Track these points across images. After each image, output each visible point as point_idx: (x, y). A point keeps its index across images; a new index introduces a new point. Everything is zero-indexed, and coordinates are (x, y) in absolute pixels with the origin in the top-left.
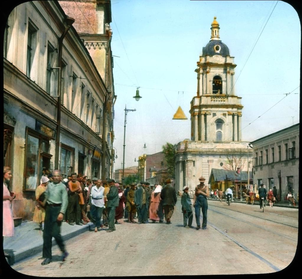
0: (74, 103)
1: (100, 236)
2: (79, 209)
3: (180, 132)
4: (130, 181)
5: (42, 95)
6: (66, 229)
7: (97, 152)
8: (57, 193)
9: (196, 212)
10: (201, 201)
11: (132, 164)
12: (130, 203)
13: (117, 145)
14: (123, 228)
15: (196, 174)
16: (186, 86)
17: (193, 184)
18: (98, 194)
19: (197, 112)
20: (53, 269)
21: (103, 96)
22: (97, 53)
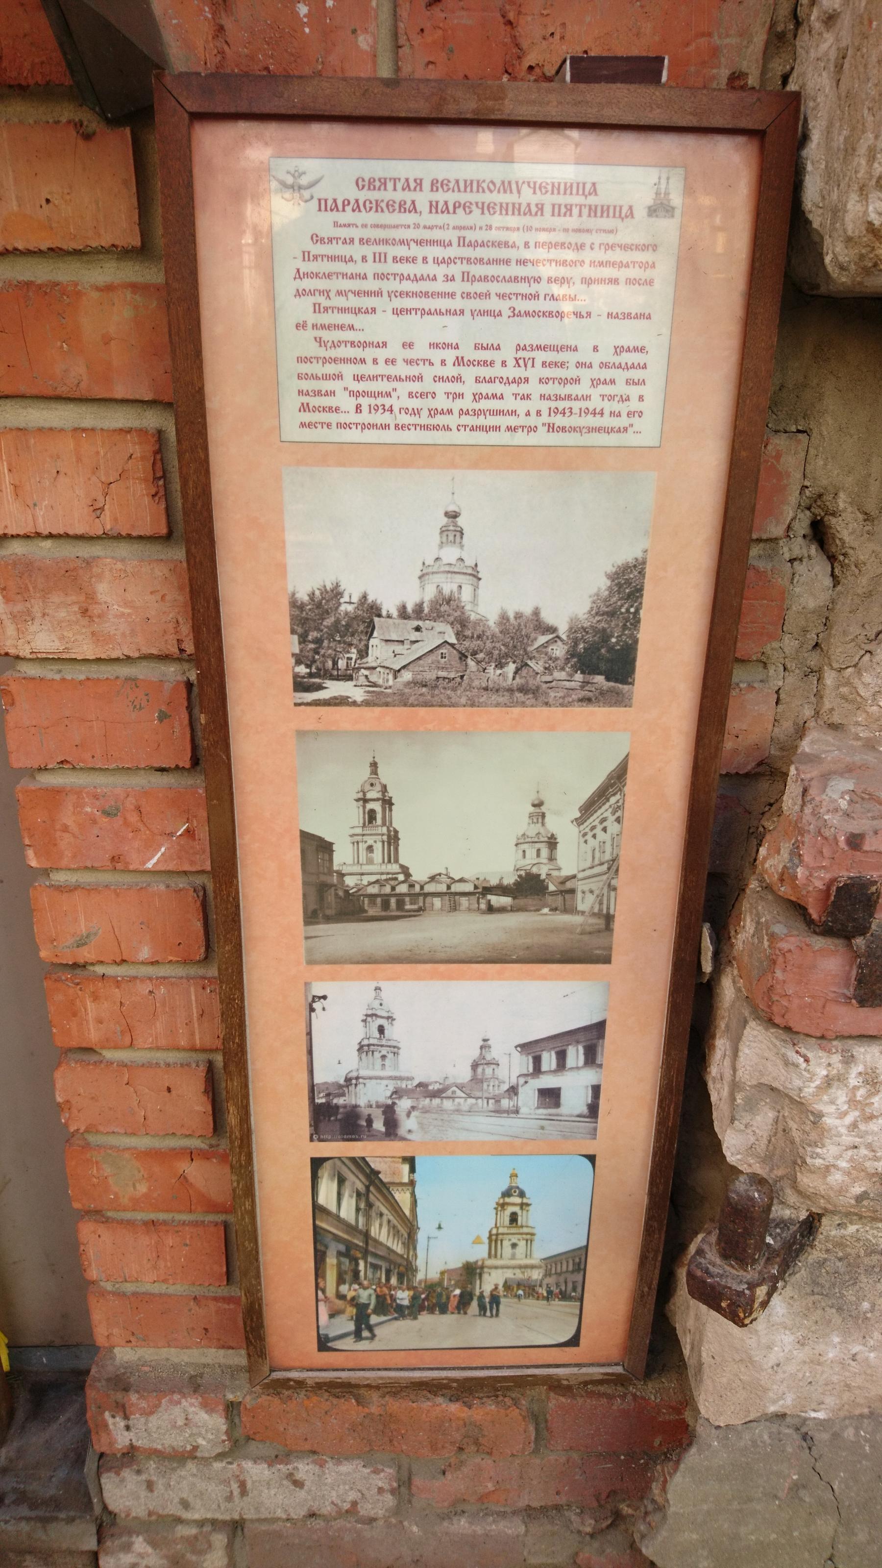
0: (381, 1233)
1: (405, 1324)
2: (385, 1305)
3: (479, 1253)
4: (431, 1287)
5: (351, 1229)
6: (374, 1319)
7: (404, 1269)
8: (366, 1296)
9: (491, 1305)
10: (495, 1299)
11: (433, 1275)
12: (432, 1300)
13: (420, 1263)
14: (425, 1318)
15: (490, 1282)
16: (486, 1220)
17: (487, 1288)
18: (403, 1297)
19: (494, 1239)
20: (363, 1345)
21: (408, 1229)
22: (402, 1198)
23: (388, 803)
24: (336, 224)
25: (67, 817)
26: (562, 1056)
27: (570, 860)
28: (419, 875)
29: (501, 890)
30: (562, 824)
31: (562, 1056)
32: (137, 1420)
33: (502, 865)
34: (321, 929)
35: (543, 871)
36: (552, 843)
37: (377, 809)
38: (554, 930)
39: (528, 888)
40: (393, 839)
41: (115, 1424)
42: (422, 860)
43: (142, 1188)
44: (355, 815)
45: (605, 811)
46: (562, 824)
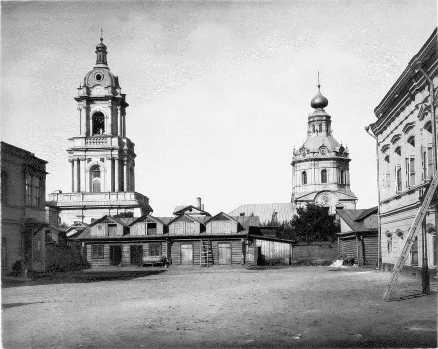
23: (119, 103)
26: (211, 257)
27: (370, 185)
28: (162, 210)
29: (275, 232)
30: (352, 128)
31: (211, 257)
33: (274, 194)
34: (26, 292)
35: (332, 203)
36: (342, 161)
37: (105, 110)
38: (352, 294)
39: (313, 228)
40: (126, 156)
42: (168, 185)
44: (75, 121)
45: (410, 113)
46: (352, 128)
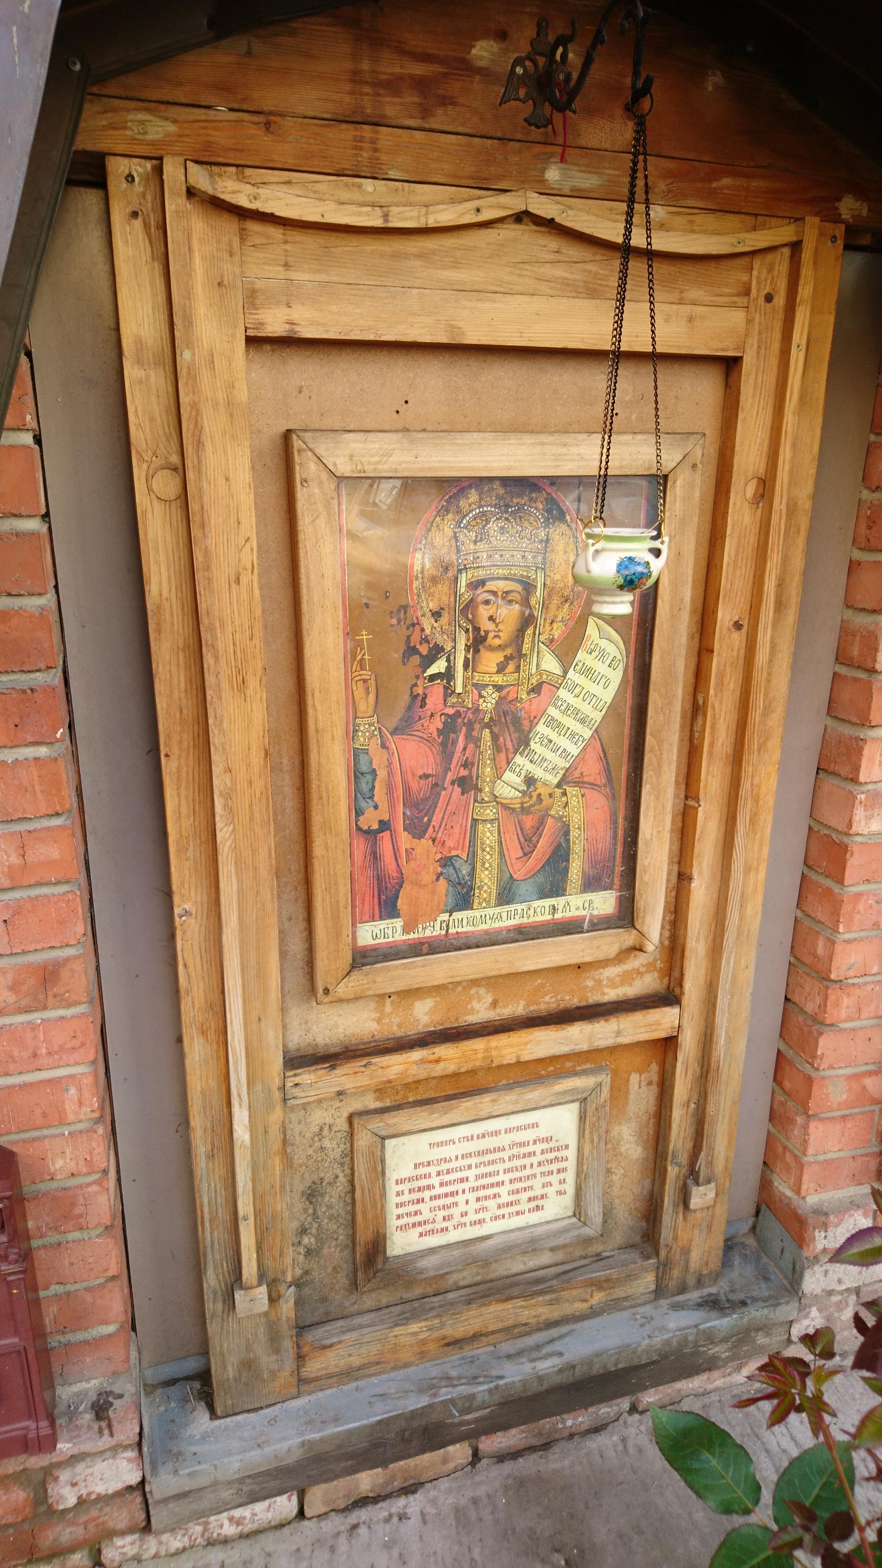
24: (535, 1125)
25: (861, 907)
32: (830, 1233)
41: (819, 1235)
43: (844, 1097)
